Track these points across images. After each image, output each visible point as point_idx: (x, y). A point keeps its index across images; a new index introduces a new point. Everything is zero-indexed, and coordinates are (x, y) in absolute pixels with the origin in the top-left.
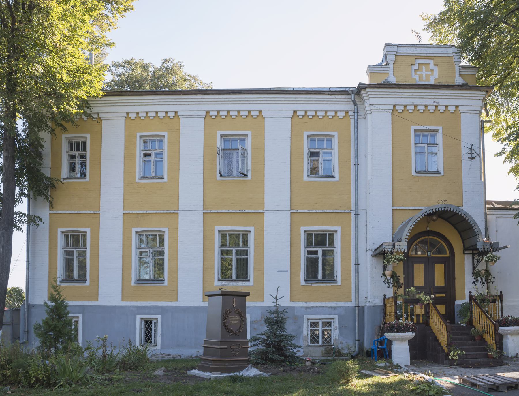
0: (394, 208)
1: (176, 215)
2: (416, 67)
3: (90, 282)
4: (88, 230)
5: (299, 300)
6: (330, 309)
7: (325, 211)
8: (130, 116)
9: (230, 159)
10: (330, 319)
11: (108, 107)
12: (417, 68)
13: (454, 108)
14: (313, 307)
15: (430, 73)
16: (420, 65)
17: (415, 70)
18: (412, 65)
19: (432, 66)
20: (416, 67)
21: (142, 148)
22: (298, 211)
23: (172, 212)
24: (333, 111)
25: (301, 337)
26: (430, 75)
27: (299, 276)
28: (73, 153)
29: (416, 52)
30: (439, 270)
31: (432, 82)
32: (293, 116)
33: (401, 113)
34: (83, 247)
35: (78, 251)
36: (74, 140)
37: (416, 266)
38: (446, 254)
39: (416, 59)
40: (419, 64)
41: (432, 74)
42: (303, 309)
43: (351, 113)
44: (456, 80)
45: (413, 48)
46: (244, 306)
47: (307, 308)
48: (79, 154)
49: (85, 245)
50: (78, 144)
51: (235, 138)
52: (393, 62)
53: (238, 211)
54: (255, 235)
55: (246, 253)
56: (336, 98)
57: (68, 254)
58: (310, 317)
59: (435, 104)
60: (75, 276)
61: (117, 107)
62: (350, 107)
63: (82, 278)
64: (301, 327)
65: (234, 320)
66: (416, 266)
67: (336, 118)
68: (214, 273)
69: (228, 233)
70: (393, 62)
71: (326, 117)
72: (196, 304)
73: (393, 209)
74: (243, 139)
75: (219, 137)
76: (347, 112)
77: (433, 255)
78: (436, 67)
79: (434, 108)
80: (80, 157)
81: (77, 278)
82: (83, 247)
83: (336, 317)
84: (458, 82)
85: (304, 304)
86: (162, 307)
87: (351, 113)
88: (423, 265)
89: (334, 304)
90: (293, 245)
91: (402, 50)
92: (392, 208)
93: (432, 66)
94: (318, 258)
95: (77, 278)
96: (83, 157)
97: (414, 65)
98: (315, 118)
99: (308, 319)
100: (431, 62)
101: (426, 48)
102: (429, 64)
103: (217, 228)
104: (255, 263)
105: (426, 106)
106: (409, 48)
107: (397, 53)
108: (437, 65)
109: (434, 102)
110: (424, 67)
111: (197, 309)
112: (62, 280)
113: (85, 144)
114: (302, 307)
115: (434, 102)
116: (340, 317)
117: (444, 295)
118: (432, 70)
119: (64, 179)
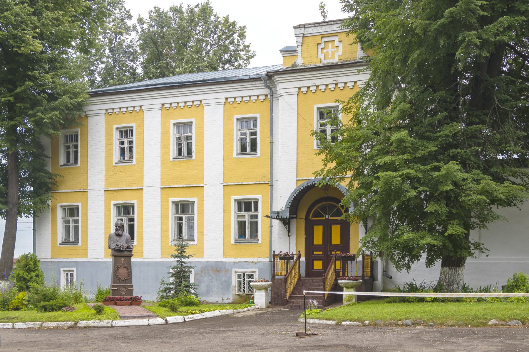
0: (298, 179)
1: (142, 190)
2: (323, 46)
3: (82, 243)
4: (80, 204)
5: (230, 256)
6: (252, 264)
7: (249, 183)
8: (203, 103)
9: (190, 141)
10: (252, 272)
11: (111, 104)
12: (323, 47)
13: (353, 84)
14: (239, 262)
15: (335, 49)
16: (326, 43)
17: (322, 48)
18: (318, 44)
19: (337, 43)
20: (323, 46)
21: (239, 128)
22: (229, 184)
23: (139, 188)
24: (255, 95)
25: (231, 287)
26: (335, 51)
27: (230, 236)
28: (68, 144)
29: (322, 31)
30: (336, 231)
31: (335, 60)
32: (225, 103)
33: (333, 90)
34: (182, 213)
35: (74, 220)
36: (68, 134)
37: (316, 227)
38: (312, 217)
39: (322, 37)
40: (325, 42)
41: (337, 51)
42: (233, 263)
43: (269, 97)
44: (358, 54)
45: (318, 27)
46: (130, 262)
47: (235, 263)
48: (73, 145)
49: (192, 212)
50: (126, 132)
51: (184, 124)
52: (301, 44)
53: (185, 186)
54: (198, 204)
55: (256, 217)
56: (256, 84)
57: (67, 222)
58: (237, 270)
59: (335, 82)
60: (72, 239)
61: (98, 105)
62: (266, 91)
63: (77, 241)
64: (230, 278)
65: (123, 272)
66: (316, 227)
67: (258, 101)
68: (169, 235)
69: (130, 205)
70: (301, 44)
71: (193, 106)
72: (157, 260)
73: (297, 180)
74: (189, 124)
75: (172, 125)
76: (266, 95)
77: (330, 218)
78: (341, 43)
79: (334, 86)
80: (74, 147)
81: (73, 241)
82: (182, 213)
83: (257, 270)
84: (359, 56)
85: (233, 260)
86: (77, 262)
87: (269, 97)
88: (322, 226)
89: (255, 260)
90: (226, 211)
91: (309, 31)
92: (296, 179)
93: (337, 43)
94: (245, 222)
95: (73, 241)
96: (131, 142)
97: (320, 44)
98: (242, 103)
99: (236, 272)
100: (336, 39)
101: (330, 26)
102: (335, 41)
103: (233, 198)
104: (198, 227)
105: (327, 85)
106: (315, 28)
107: (304, 34)
108: (341, 41)
109: (333, 80)
110: (330, 45)
111: (157, 264)
112: (63, 242)
113: (132, 131)
114: (232, 262)
115: (333, 80)
116: (259, 270)
117: (321, 253)
118: (338, 46)
119: (61, 166)
